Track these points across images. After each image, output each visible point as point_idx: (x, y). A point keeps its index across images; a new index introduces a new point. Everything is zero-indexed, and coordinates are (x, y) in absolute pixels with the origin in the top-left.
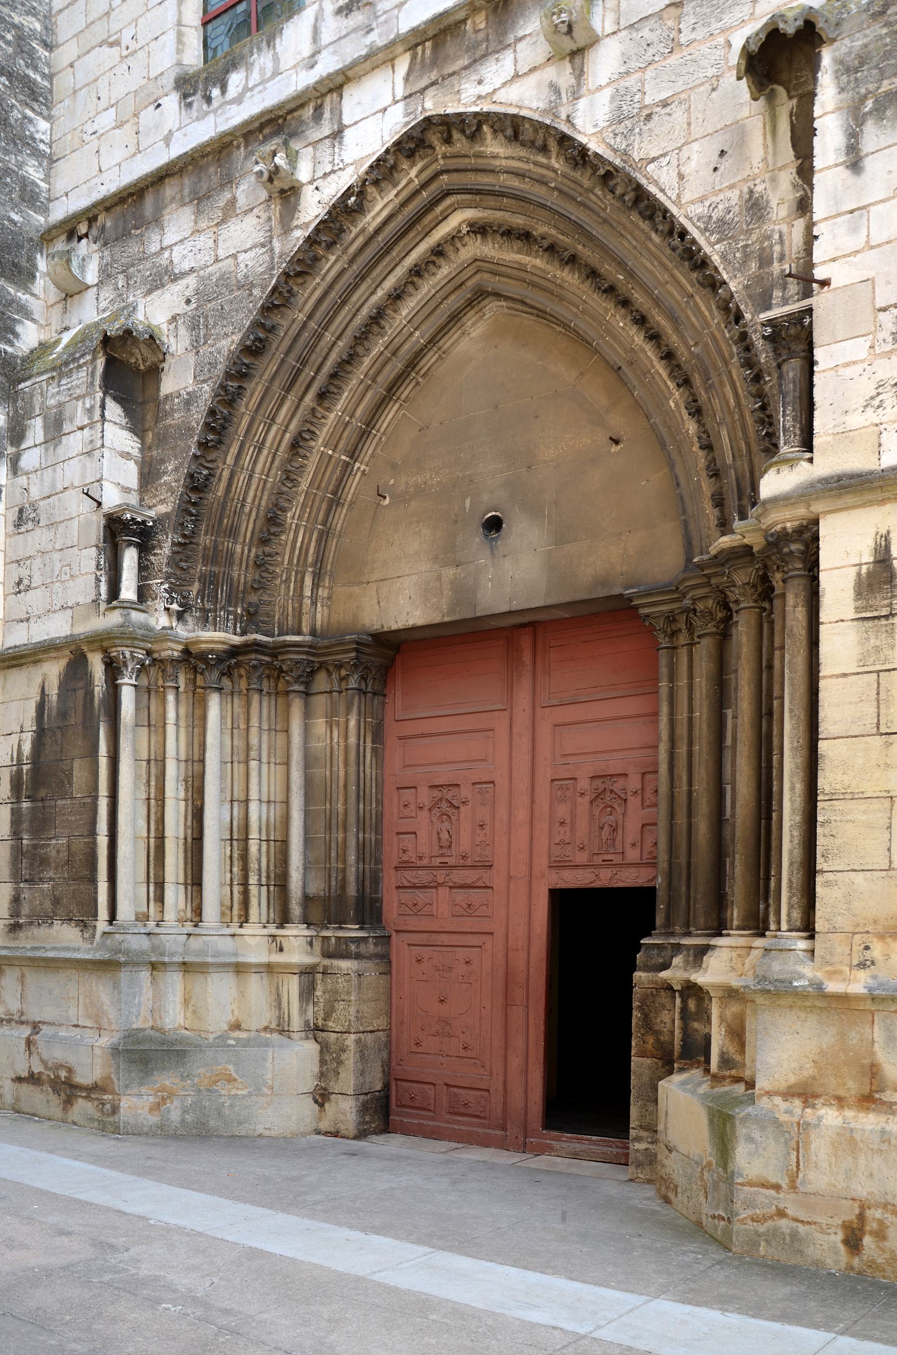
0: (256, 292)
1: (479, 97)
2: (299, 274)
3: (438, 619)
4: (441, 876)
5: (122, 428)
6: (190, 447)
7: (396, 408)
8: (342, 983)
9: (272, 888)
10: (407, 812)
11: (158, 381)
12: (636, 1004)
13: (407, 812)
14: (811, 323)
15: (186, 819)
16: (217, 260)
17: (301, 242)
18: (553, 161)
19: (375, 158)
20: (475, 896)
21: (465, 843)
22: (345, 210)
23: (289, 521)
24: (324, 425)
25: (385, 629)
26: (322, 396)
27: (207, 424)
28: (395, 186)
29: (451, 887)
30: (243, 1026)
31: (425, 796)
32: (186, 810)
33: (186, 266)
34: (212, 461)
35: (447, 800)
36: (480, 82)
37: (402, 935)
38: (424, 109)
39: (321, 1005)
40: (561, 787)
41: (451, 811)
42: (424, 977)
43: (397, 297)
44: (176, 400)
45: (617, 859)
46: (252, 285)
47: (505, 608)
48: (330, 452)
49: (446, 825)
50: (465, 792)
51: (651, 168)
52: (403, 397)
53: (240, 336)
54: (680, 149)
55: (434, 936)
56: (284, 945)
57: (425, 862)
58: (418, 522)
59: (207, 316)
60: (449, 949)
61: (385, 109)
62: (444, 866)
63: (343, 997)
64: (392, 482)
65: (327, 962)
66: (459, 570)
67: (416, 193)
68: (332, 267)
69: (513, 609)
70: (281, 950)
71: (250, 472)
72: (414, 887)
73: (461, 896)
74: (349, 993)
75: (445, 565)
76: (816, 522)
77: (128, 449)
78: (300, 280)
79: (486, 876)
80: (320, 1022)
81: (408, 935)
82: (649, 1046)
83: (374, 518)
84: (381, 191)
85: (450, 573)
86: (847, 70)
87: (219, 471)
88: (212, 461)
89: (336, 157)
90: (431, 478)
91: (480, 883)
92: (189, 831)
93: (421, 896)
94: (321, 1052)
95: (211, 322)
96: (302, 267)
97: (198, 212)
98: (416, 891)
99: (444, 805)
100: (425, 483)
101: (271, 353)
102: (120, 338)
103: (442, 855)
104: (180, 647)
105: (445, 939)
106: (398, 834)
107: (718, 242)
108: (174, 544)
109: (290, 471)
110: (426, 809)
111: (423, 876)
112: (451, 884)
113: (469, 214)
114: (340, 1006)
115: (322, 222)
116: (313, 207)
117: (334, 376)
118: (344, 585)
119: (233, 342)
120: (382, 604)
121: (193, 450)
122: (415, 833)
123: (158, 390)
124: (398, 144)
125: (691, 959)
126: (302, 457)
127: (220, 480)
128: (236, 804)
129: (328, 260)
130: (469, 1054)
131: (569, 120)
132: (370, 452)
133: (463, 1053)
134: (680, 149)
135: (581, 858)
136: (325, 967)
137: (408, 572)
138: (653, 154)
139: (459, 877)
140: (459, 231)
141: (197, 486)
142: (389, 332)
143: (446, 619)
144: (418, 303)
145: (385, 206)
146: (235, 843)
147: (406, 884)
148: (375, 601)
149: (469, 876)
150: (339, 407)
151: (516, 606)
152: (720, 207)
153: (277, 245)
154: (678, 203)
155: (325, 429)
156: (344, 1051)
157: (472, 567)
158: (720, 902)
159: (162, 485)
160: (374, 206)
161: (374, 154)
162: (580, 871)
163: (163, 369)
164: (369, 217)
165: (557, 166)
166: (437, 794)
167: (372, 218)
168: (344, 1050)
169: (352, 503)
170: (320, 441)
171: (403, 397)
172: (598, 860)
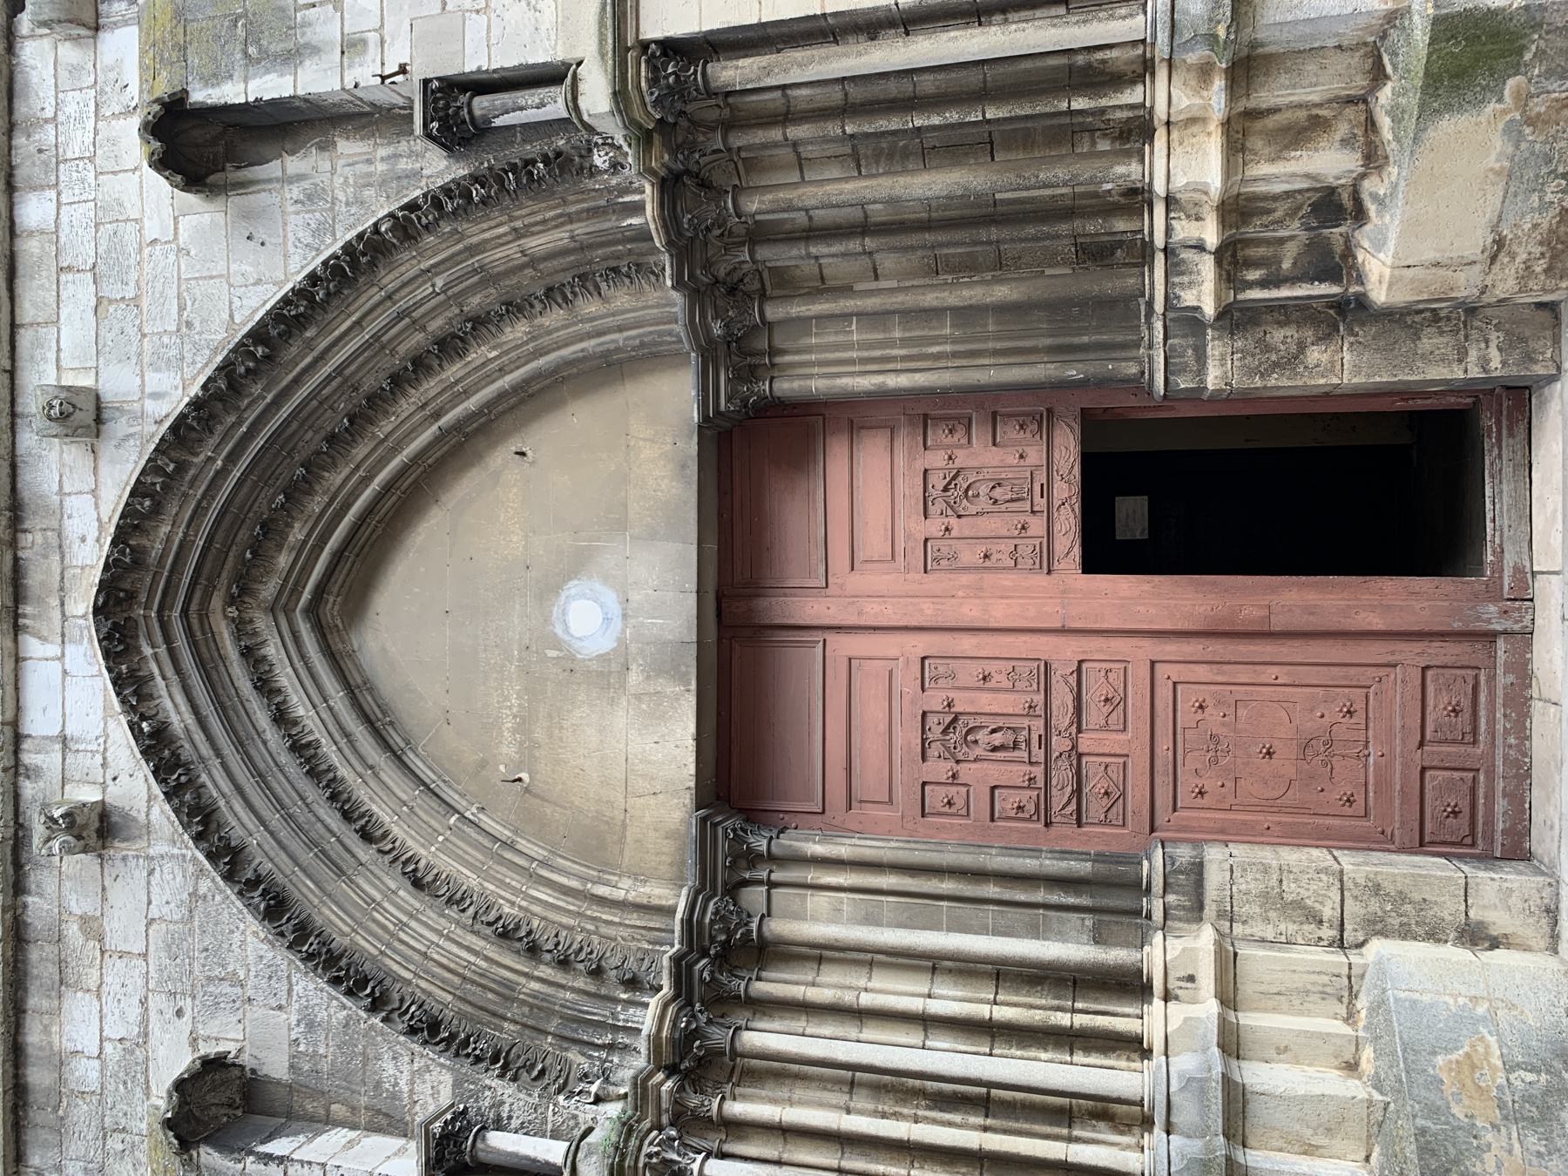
0: (204, 886)
1: (98, 540)
2: (205, 822)
3: (692, 700)
4: (1059, 744)
5: (310, 1140)
6: (372, 1027)
7: (411, 755)
8: (1248, 883)
9: (1079, 1005)
10: (960, 802)
11: (268, 1081)
12: (1258, 382)
13: (960, 802)
14: (438, 79)
15: (950, 1124)
16: (145, 956)
17: (167, 807)
18: (196, 460)
19: (110, 686)
20: (1094, 691)
21: (1010, 703)
22: (157, 746)
23: (515, 911)
24: (403, 844)
25: (692, 784)
26: (366, 836)
27: (349, 993)
28: (152, 678)
29: (1079, 731)
30: (1348, 1056)
31: (939, 769)
32: (935, 1121)
33: (134, 1012)
34: (402, 1000)
35: (945, 732)
36: (83, 540)
37: (1158, 823)
38: (84, 616)
39: (1292, 928)
40: (937, 560)
41: (961, 727)
42: (1230, 784)
43: (281, 717)
44: (302, 1048)
45: (1041, 477)
46: (194, 894)
47: (692, 600)
48: (441, 839)
49: (981, 736)
50: (935, 700)
51: (238, 320)
52: (402, 745)
53: (250, 918)
54: (231, 285)
55: (1158, 763)
56: (1183, 974)
57: (1038, 771)
58: (562, 728)
59: (209, 978)
60: (1179, 737)
61: (65, 672)
62: (1045, 741)
63: (1274, 882)
64: (502, 768)
65: (1210, 910)
66: (634, 667)
67: (172, 652)
68: (214, 781)
69: (695, 588)
70: (1191, 979)
71: (427, 947)
72: (1078, 791)
73: (1094, 714)
74: (1266, 870)
75: (623, 685)
76: (644, 46)
77: (344, 1141)
78: (213, 826)
79: (1062, 671)
80: (1328, 933)
81: (1158, 813)
82: (1325, 358)
83: (544, 799)
84: (151, 697)
85: (634, 678)
86: (215, 77)
87: (419, 993)
88: (402, 1000)
89: (89, 748)
90: (510, 708)
91: (1073, 680)
92: (973, 1120)
93: (1095, 783)
94: (1383, 934)
95: (217, 971)
96: (201, 820)
97: (78, 986)
98: (1085, 790)
99: (953, 737)
100: (515, 717)
101: (289, 886)
102: (183, 1103)
103: (1028, 742)
104: (660, 1076)
105: (1163, 745)
106: (992, 820)
107: (334, 234)
108: (501, 1076)
109: (450, 899)
110: (956, 768)
111: (1062, 774)
112: (1074, 729)
113: (217, 602)
114: (1292, 890)
115: (155, 773)
116: (132, 785)
117: (347, 816)
118: (622, 851)
119: (255, 933)
120: (658, 788)
121: (376, 1020)
122: (993, 788)
123: (279, 1082)
124: (107, 655)
125: (1186, 279)
126: (434, 881)
127: (429, 994)
128: (928, 1043)
129: (203, 786)
130: (1359, 706)
131: (159, 422)
132: (456, 797)
133: (1359, 718)
134: (231, 285)
135: (1037, 526)
136: (1221, 915)
137: (622, 746)
138: (226, 316)
139: (1062, 718)
140: (233, 619)
141: (428, 1029)
142: (317, 735)
143: (693, 686)
144: (296, 692)
145: (170, 696)
146: (1000, 998)
147: (1073, 806)
148: (652, 801)
149: (1062, 697)
150: (387, 819)
151: (692, 585)
152: (300, 235)
153: (158, 848)
154: (280, 284)
155: (410, 842)
156: (1378, 887)
157: (633, 648)
158: (1106, 207)
159: (411, 1091)
160: (165, 710)
161: (106, 689)
162: (1057, 527)
163: (253, 1071)
164: (174, 719)
165: (202, 457)
166: (934, 751)
167: (178, 716)
168: (1377, 889)
169: (516, 832)
170: (423, 852)
171: (402, 745)
172: (1041, 503)
